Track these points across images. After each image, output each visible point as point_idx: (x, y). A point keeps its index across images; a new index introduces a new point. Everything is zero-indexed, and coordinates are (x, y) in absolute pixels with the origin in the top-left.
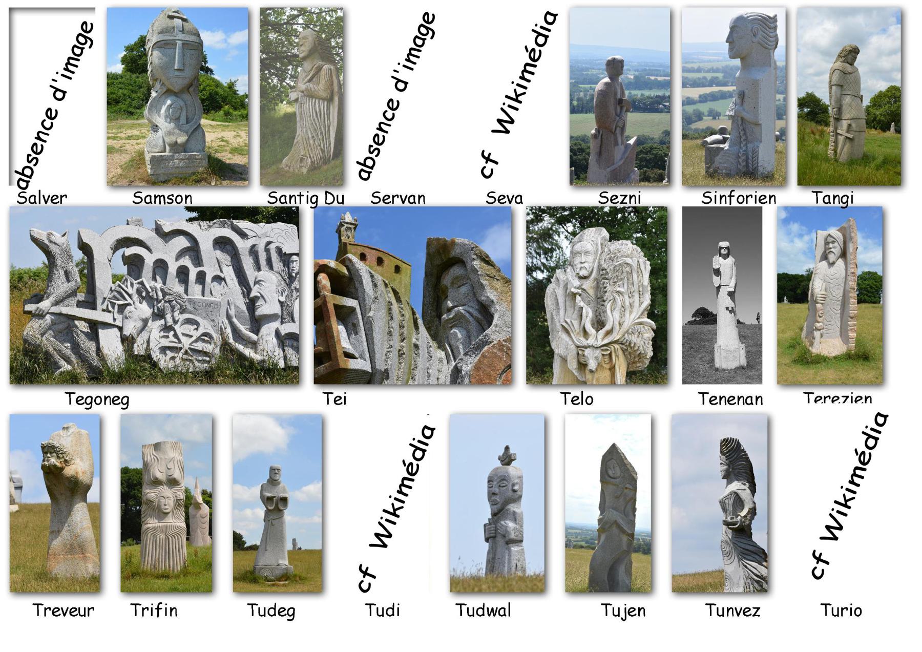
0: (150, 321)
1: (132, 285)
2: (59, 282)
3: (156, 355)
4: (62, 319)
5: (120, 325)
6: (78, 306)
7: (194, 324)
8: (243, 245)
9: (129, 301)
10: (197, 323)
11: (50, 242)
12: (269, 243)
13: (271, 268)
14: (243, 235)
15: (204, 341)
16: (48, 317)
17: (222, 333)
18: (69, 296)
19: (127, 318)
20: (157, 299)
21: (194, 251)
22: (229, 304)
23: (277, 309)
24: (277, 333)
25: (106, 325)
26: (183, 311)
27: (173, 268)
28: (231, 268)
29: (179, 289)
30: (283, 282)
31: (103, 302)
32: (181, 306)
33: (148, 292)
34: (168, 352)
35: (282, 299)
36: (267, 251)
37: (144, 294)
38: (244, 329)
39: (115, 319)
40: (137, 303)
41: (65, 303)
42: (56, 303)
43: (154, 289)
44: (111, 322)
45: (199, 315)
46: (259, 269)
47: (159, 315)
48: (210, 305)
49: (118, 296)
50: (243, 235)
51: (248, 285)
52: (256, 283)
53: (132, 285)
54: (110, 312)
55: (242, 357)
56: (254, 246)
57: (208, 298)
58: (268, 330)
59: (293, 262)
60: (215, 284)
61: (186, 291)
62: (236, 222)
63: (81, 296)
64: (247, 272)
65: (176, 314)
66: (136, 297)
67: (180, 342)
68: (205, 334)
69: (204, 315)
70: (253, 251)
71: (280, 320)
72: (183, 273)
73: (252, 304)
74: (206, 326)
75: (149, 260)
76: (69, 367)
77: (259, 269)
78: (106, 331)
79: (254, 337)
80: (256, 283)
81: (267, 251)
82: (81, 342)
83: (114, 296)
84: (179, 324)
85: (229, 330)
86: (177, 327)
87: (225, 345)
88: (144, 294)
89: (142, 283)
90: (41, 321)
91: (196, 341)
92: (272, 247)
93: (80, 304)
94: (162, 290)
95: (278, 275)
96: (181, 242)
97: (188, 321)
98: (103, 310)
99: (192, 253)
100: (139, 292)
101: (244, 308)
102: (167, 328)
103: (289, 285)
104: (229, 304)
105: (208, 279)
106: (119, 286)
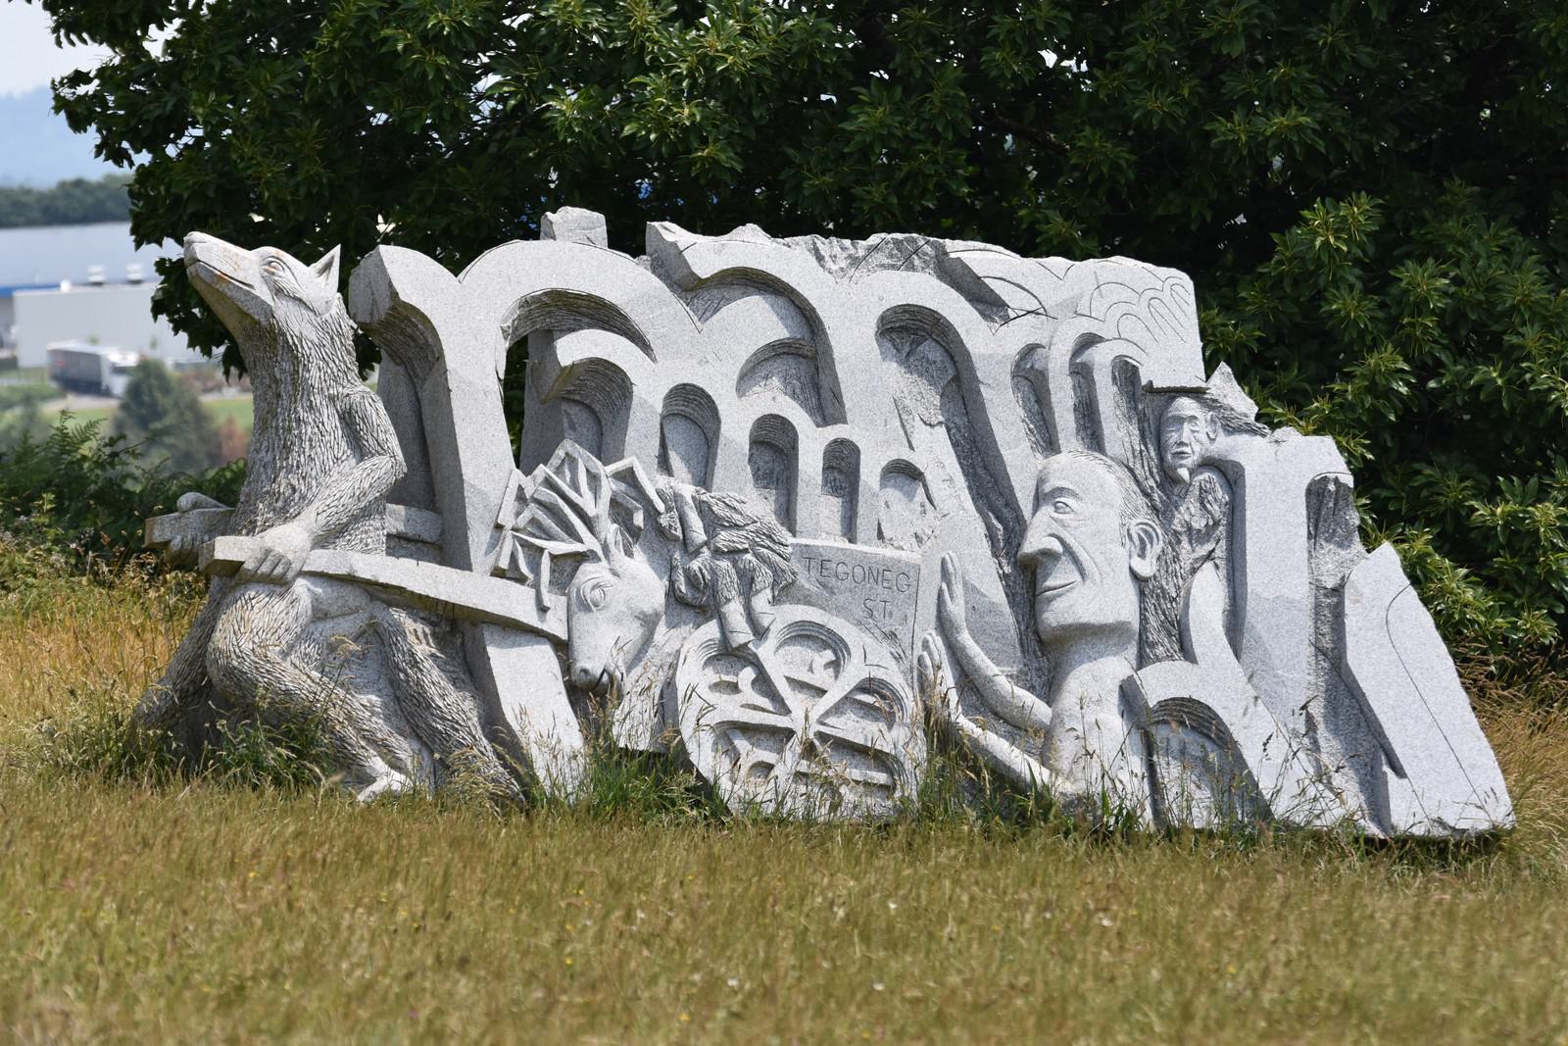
0: (661, 628)
1: (594, 479)
2: (323, 455)
3: (705, 757)
4: (352, 597)
5: (561, 633)
6: (391, 551)
7: (825, 645)
8: (989, 346)
9: (590, 543)
10: (835, 644)
11: (278, 291)
12: (1089, 341)
13: (1093, 437)
14: (987, 302)
15: (869, 711)
16: (301, 587)
17: (924, 686)
18: (366, 513)
19: (586, 607)
20: (685, 543)
21: (805, 356)
22: (945, 574)
23: (1123, 606)
24: (1129, 697)
25: (514, 629)
26: (785, 591)
27: (737, 423)
28: (941, 432)
29: (759, 506)
30: (1141, 501)
31: (495, 543)
32: (777, 572)
33: (652, 514)
34: (742, 744)
35: (1146, 568)
36: (1082, 373)
37: (639, 519)
38: (1001, 677)
39: (543, 610)
40: (618, 553)
41: (356, 535)
42: (327, 538)
43: (674, 501)
44: (530, 618)
45: (839, 610)
46: (1049, 444)
47: (694, 602)
48: (877, 573)
49: (548, 522)
50: (987, 302)
51: (1011, 503)
52: (1040, 499)
53: (594, 479)
54: (521, 579)
55: (1004, 777)
56: (1031, 349)
57: (866, 547)
58: (1095, 680)
59: (1180, 420)
60: (893, 494)
61: (787, 515)
62: (956, 248)
63: (396, 518)
64: (1007, 454)
65: (761, 602)
66: (610, 530)
67: (783, 709)
68: (868, 686)
69: (859, 612)
70: (1029, 376)
71: (1132, 651)
72: (773, 445)
73: (1027, 577)
74: (870, 657)
75: (650, 386)
76: (396, 781)
77: (1049, 444)
78: (514, 652)
79: (1042, 711)
80: (1040, 499)
81: (1082, 373)
82: (432, 691)
83: (533, 521)
84: (772, 640)
85: (948, 677)
86: (765, 652)
87: (942, 737)
88: (639, 519)
89: (628, 477)
90: (279, 606)
91: (837, 709)
92: (1101, 358)
93: (400, 544)
94: (703, 509)
95: (1124, 474)
96: (756, 322)
97: (804, 634)
98: (498, 573)
99: (790, 365)
100: (619, 511)
101: (997, 594)
102: (729, 654)
103: (1163, 513)
104: (945, 574)
105: (870, 473)
106: (549, 483)
